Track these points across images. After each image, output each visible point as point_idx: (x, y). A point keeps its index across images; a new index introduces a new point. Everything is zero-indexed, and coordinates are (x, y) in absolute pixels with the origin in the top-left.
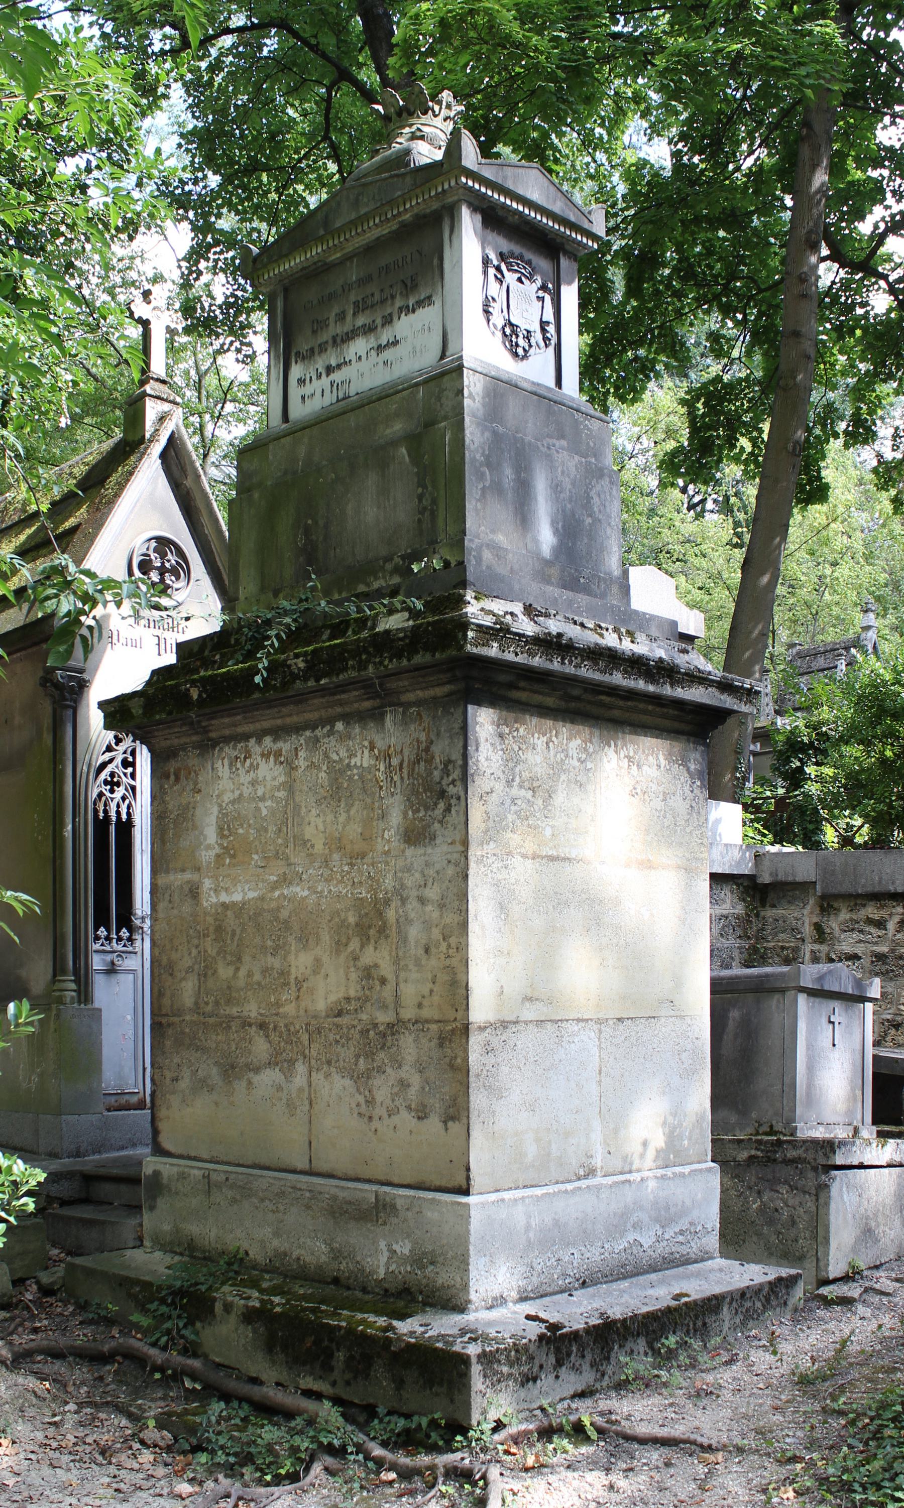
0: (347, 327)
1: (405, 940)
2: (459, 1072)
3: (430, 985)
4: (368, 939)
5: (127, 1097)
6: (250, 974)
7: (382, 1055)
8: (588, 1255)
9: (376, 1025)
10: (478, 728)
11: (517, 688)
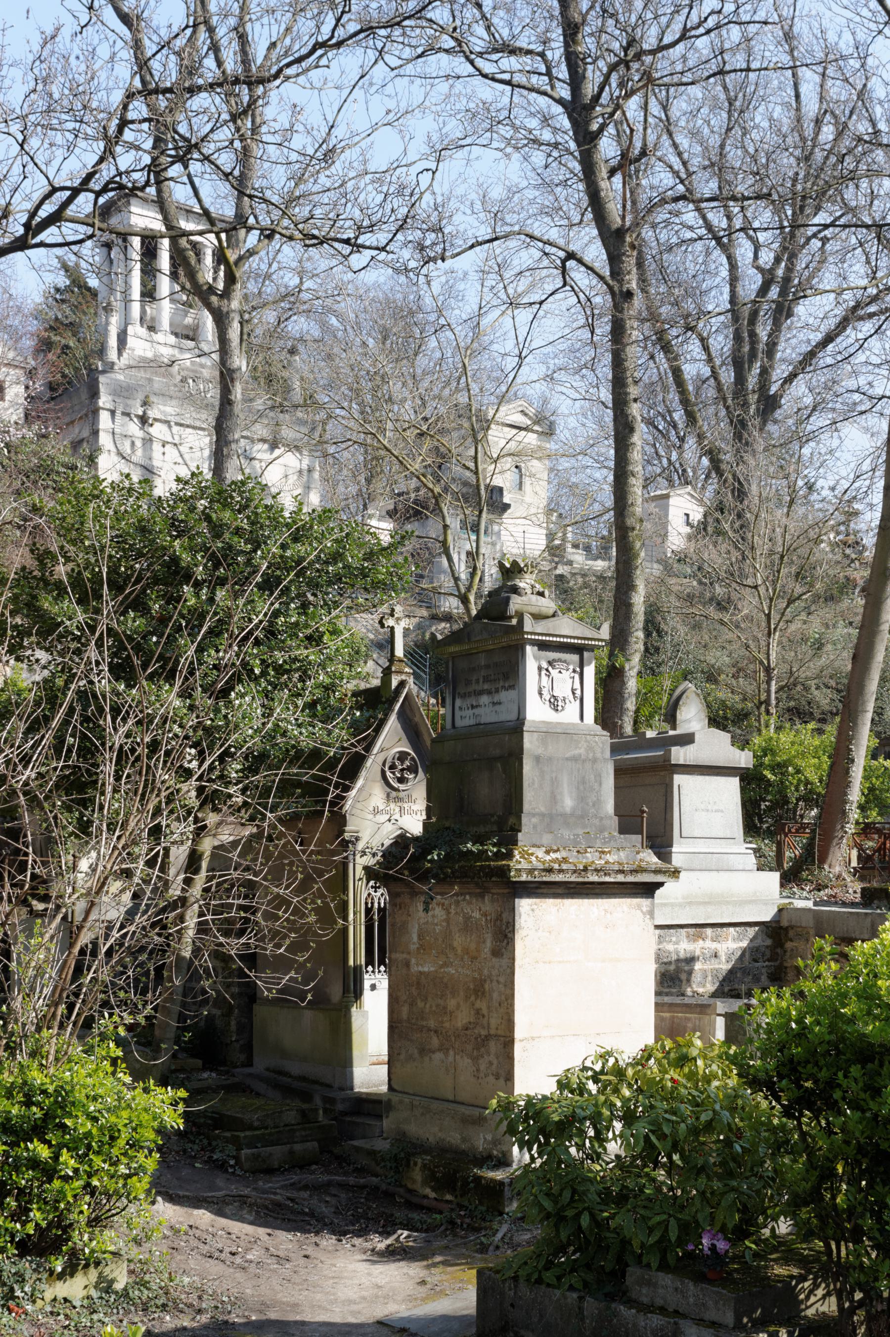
2: (510, 1058)
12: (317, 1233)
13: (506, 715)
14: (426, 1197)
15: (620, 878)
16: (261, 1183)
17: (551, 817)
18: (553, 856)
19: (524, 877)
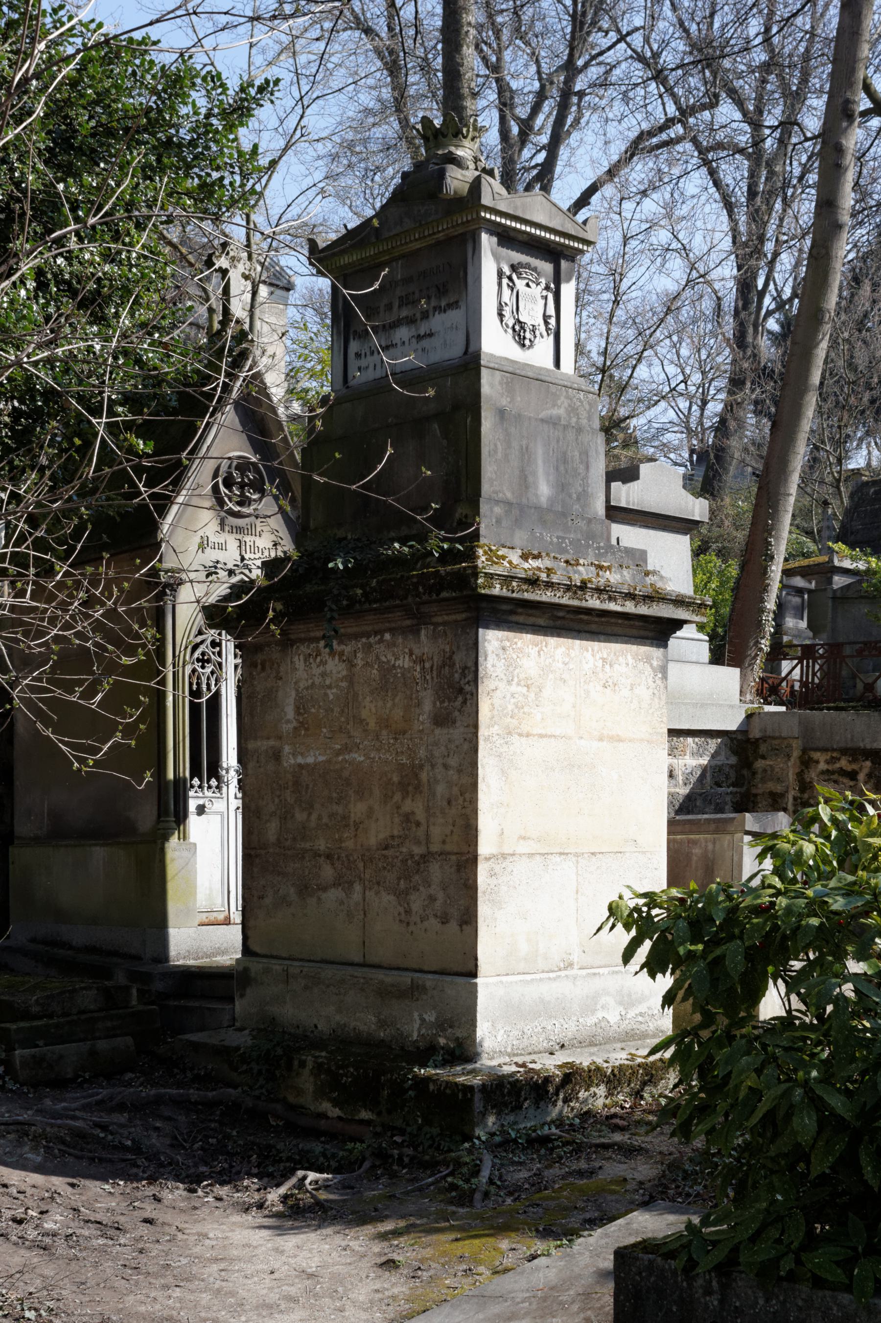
0: (394, 318)
1: (434, 795)
2: (470, 889)
3: (451, 827)
4: (407, 793)
5: (215, 914)
6: (320, 818)
7: (417, 877)
8: (566, 1026)
9: (412, 856)
10: (486, 644)
11: (515, 613)
12: (152, 1180)
13: (446, 350)
14: (323, 1116)
15: (630, 607)
16: (48, 1102)
17: (522, 508)
18: (533, 563)
19: (497, 590)
